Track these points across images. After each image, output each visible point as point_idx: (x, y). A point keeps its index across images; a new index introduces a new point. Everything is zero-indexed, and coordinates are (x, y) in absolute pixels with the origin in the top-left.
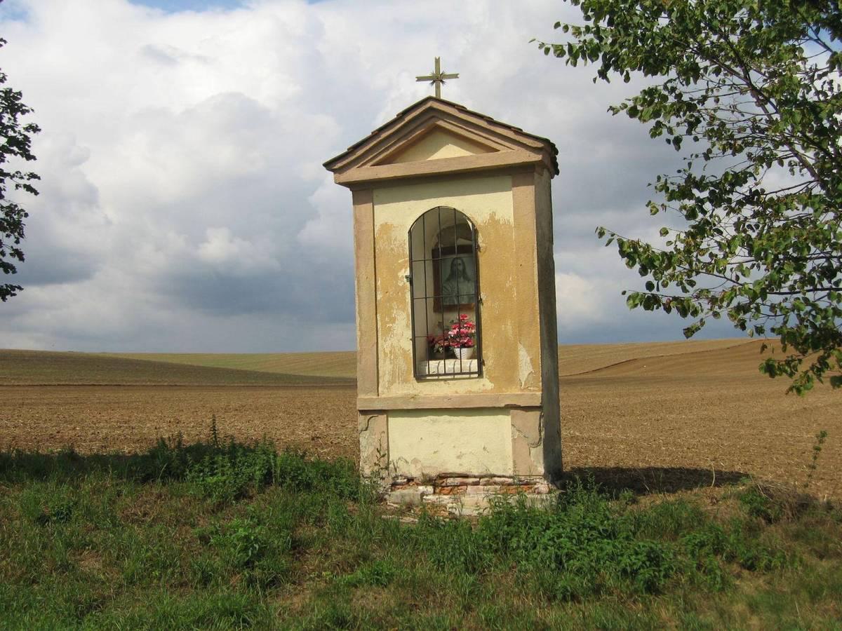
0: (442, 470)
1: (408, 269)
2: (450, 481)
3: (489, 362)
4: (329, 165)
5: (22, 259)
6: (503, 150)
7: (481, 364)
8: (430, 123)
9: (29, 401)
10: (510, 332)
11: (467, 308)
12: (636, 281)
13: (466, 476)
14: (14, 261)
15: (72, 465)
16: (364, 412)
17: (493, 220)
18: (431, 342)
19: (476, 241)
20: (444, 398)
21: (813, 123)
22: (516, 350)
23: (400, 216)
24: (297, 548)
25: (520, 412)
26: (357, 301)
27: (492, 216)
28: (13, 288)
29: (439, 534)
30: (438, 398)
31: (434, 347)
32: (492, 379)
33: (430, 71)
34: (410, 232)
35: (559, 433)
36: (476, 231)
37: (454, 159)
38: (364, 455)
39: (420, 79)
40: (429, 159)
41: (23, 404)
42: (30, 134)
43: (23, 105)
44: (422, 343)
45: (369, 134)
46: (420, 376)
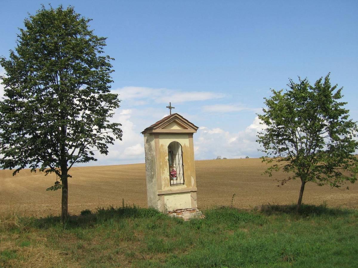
0: (177, 209)
1: (168, 157)
2: (178, 211)
6: (189, 129)
10: (189, 174)
12: (113, 141)
21: (36, 54)
25: (193, 193)
26: (156, 165)
30: (176, 190)
33: (169, 105)
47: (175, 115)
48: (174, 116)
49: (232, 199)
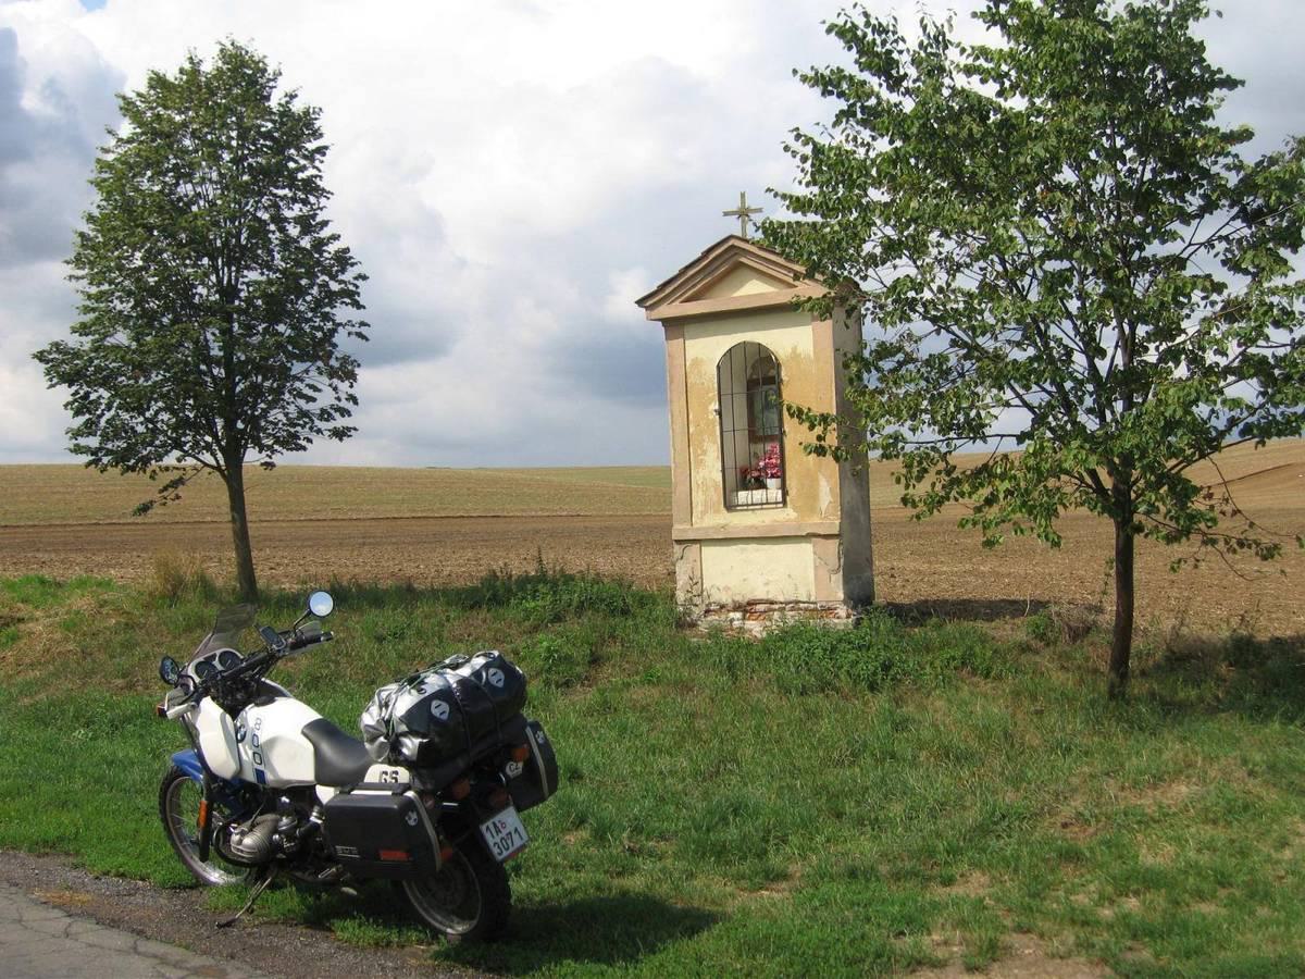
0: (750, 597)
3: (792, 492)
4: (640, 302)
5: (356, 403)
7: (785, 494)
8: (734, 259)
9: (372, 540)
11: (771, 438)
13: (772, 603)
14: (349, 405)
15: (408, 594)
16: (679, 542)
17: (795, 355)
18: (744, 472)
19: (779, 374)
20: (752, 527)
22: (817, 480)
23: (708, 350)
24: (595, 661)
27: (794, 349)
28: (349, 429)
29: (736, 657)
31: (749, 478)
32: (795, 509)
33: (735, 205)
34: (718, 367)
35: (870, 562)
36: (779, 365)
37: (756, 295)
38: (680, 584)
39: (726, 214)
40: (735, 295)
41: (364, 544)
42: (360, 283)
43: (351, 258)
44: (731, 478)
45: (676, 272)
46: (730, 506)
47: (730, 243)
48: (725, 246)
49: (1106, 584)
